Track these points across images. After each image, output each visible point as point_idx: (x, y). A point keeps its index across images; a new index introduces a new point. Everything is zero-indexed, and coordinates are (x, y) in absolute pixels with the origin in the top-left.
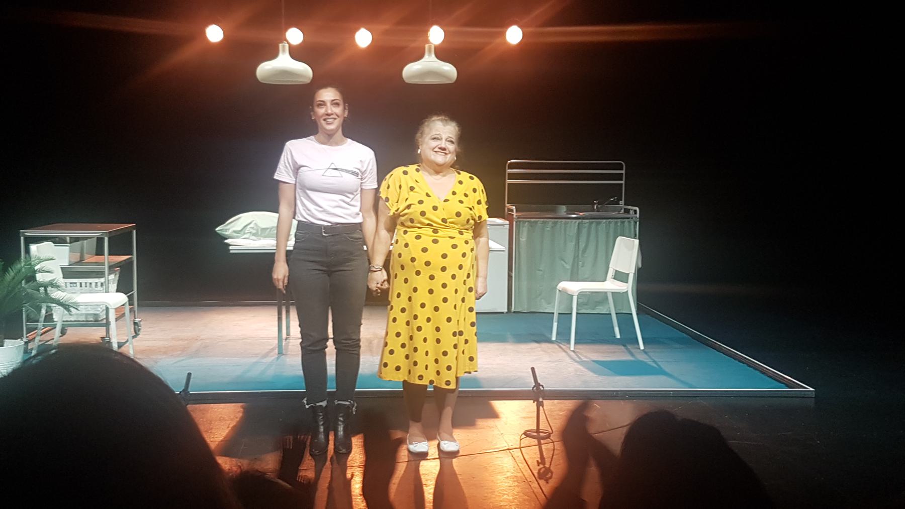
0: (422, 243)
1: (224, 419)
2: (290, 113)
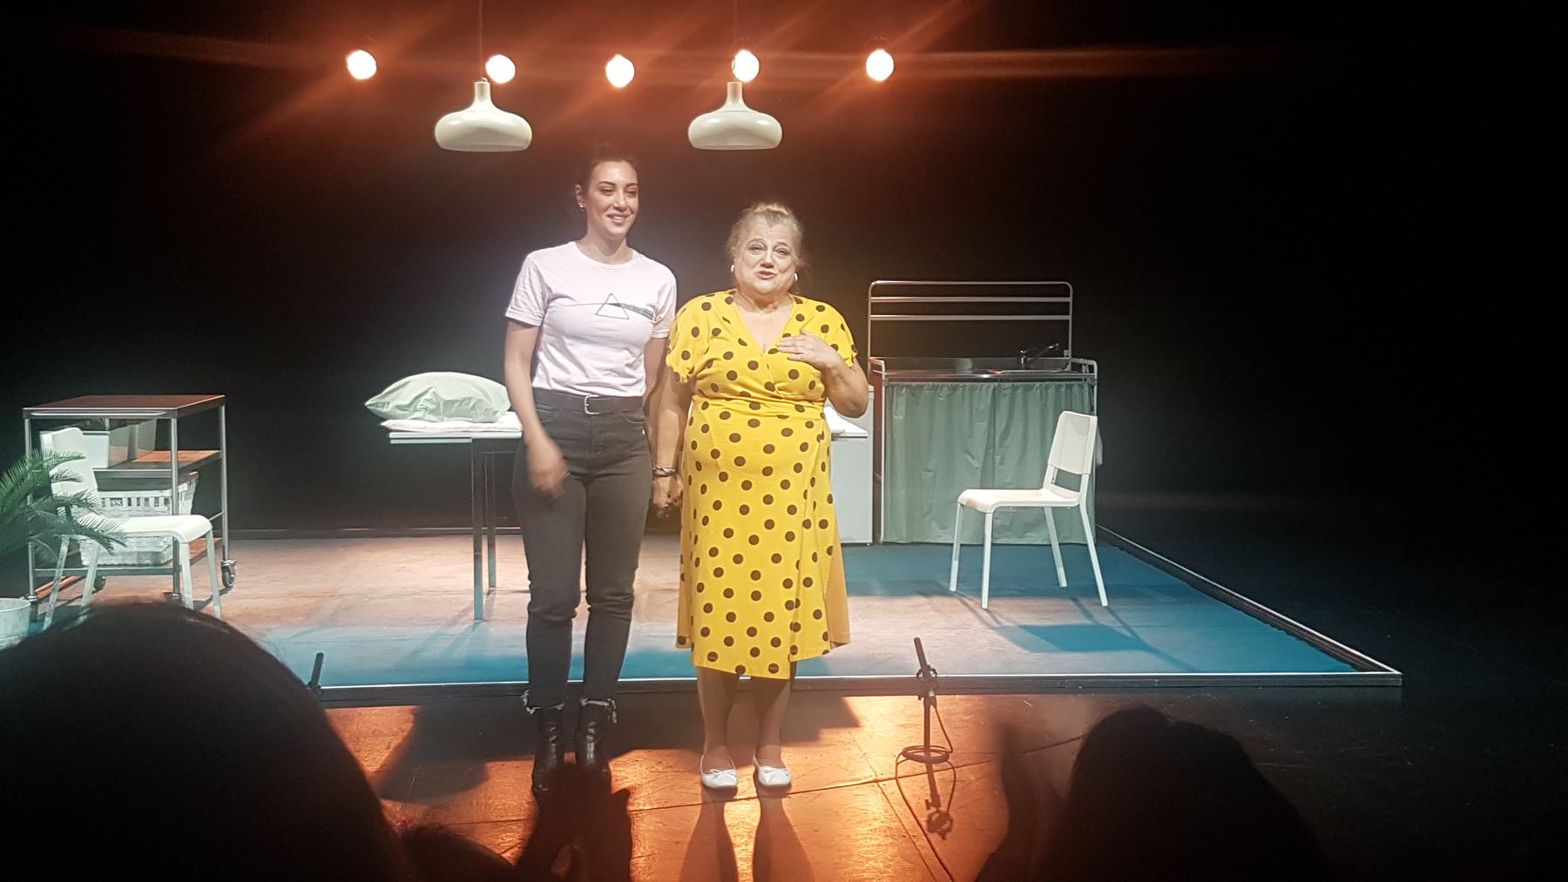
1: (381, 734)
2: (530, 199)
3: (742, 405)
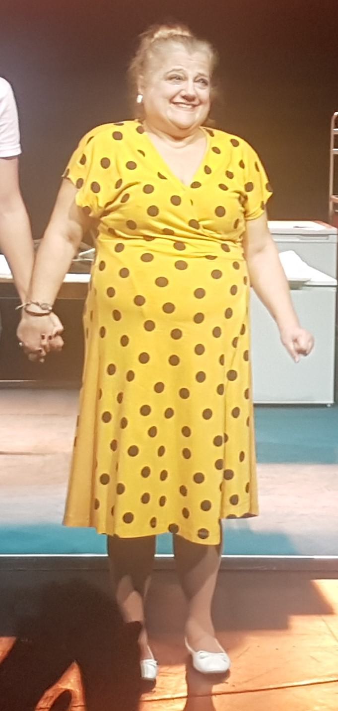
0: (154, 270)
3: (163, 245)
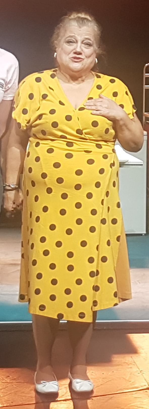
3: (60, 144)
